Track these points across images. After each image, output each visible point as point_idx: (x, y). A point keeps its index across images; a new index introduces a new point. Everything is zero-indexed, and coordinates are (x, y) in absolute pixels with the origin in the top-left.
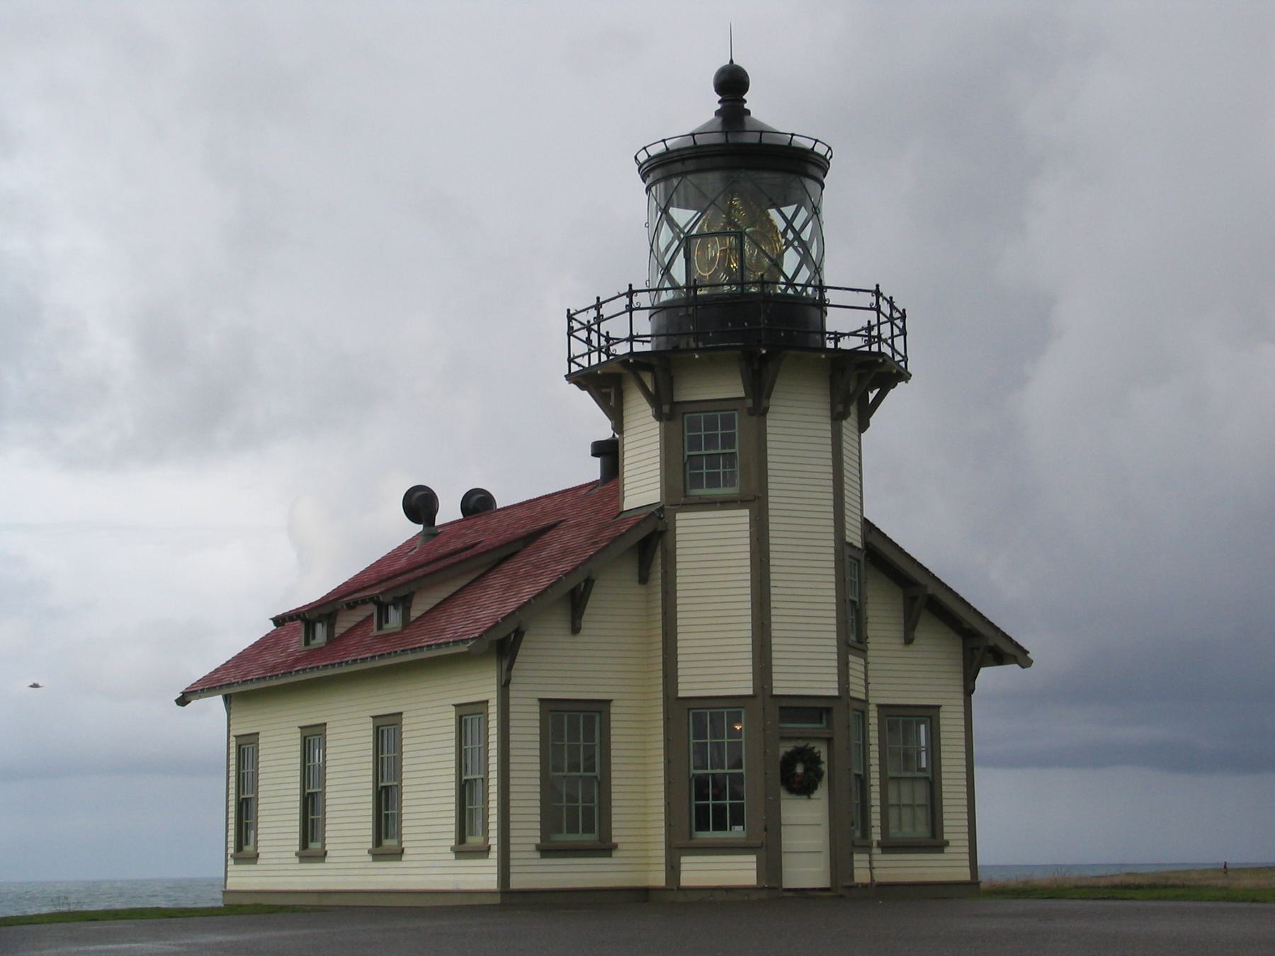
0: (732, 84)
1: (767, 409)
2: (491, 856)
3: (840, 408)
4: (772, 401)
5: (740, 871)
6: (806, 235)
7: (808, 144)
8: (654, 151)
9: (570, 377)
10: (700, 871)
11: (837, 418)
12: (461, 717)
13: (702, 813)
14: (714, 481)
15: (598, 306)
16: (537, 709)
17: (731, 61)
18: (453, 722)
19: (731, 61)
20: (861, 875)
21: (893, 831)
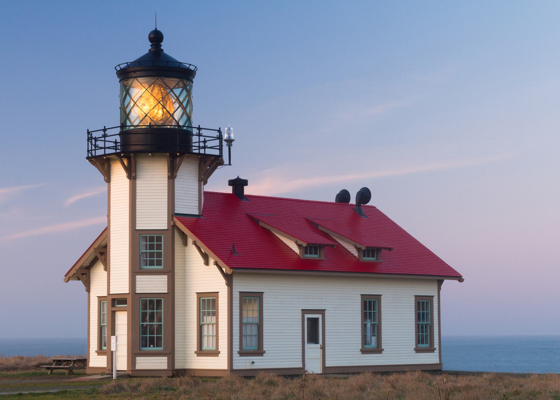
0: (156, 38)
1: (175, 177)
2: (435, 351)
3: (203, 177)
4: (178, 173)
5: (159, 363)
6: (185, 104)
7: (188, 66)
8: (122, 66)
9: (88, 158)
10: (145, 363)
11: (200, 181)
12: (419, 303)
13: (144, 339)
15: (105, 130)
16: (414, 299)
17: (156, 29)
18: (97, 303)
19: (156, 29)
20: (139, 366)
21: (244, 347)
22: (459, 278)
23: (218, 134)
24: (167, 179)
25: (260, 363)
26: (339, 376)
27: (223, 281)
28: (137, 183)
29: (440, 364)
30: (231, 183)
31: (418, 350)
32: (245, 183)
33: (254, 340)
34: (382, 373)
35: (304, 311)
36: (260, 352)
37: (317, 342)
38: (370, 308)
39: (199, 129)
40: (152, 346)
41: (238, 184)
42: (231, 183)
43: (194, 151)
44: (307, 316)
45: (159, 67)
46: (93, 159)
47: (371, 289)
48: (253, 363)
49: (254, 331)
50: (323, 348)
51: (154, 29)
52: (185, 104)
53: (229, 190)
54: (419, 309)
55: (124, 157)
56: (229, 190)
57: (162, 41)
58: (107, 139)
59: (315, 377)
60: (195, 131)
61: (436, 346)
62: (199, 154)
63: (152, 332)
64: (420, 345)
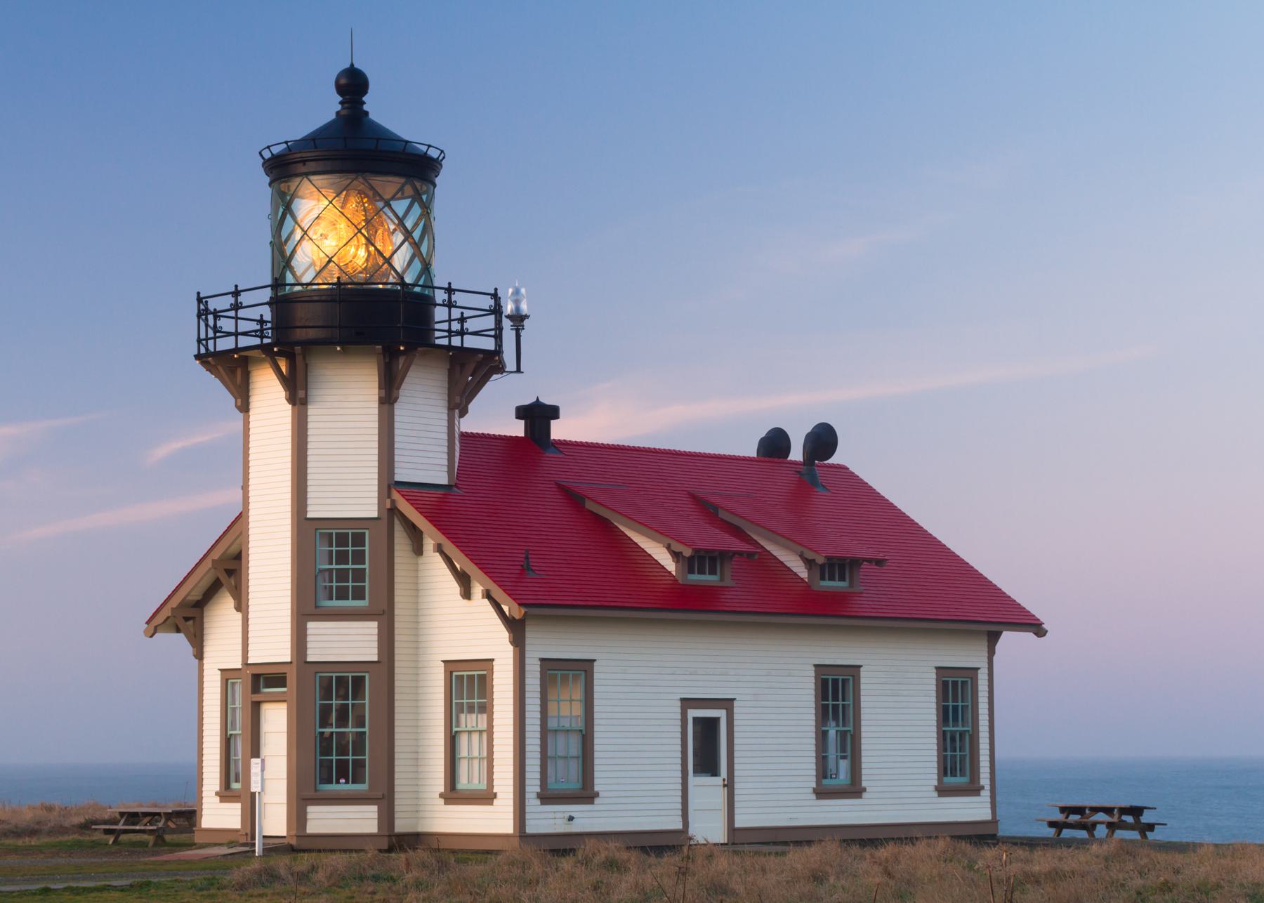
0: (353, 85)
1: (396, 400)
2: (982, 793)
3: (457, 399)
4: (401, 392)
5: (359, 820)
6: (416, 235)
7: (424, 148)
8: (276, 150)
9: (198, 357)
10: (327, 820)
11: (451, 409)
13: (325, 766)
14: (342, 595)
15: (236, 293)
17: (352, 65)
18: (219, 684)
19: (352, 65)
20: (313, 827)
22: (1037, 628)
23: (492, 302)
24: (376, 405)
25: (586, 819)
26: (765, 849)
27: (503, 634)
28: (310, 412)
29: (994, 821)
30: (522, 412)
31: (943, 791)
32: (553, 412)
33: (574, 769)
34: (863, 843)
35: (687, 703)
36: (586, 794)
37: (715, 772)
38: (836, 695)
39: (450, 290)
40: (342, 781)
41: (538, 416)
42: (522, 412)
43: (438, 342)
44: (693, 713)
45: (360, 151)
46: (209, 359)
47: (838, 652)
48: (571, 819)
49: (574, 747)
50: (729, 785)
51: (348, 66)
52: (416, 235)
53: (517, 429)
54: (945, 699)
55: (280, 354)
56: (517, 429)
57: (365, 92)
58: (241, 313)
59: (711, 851)
60: (440, 296)
61: (985, 780)
62: (449, 347)
63: (343, 750)
64: (949, 780)
